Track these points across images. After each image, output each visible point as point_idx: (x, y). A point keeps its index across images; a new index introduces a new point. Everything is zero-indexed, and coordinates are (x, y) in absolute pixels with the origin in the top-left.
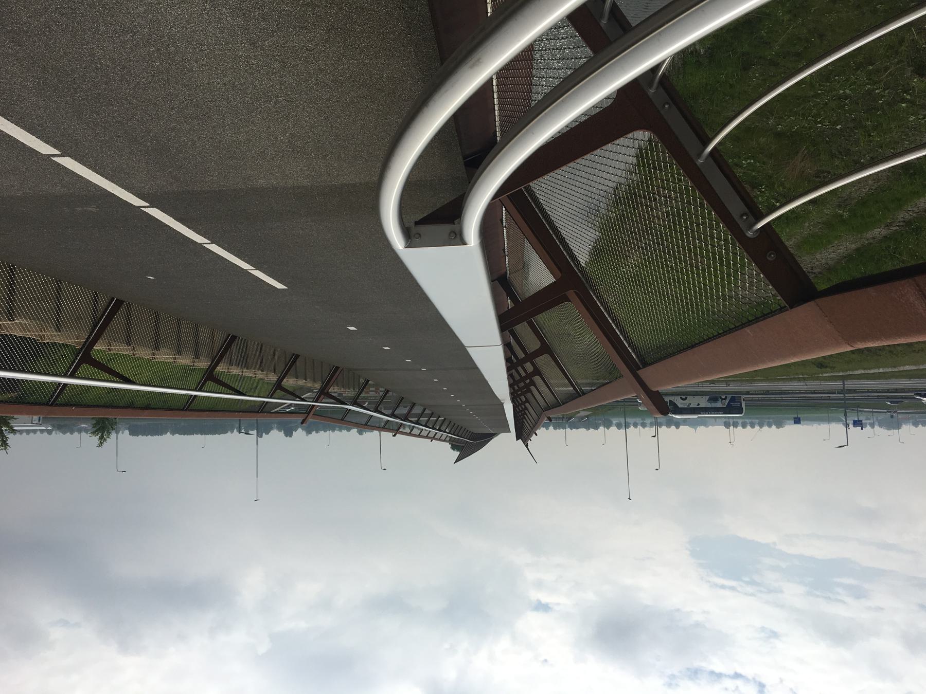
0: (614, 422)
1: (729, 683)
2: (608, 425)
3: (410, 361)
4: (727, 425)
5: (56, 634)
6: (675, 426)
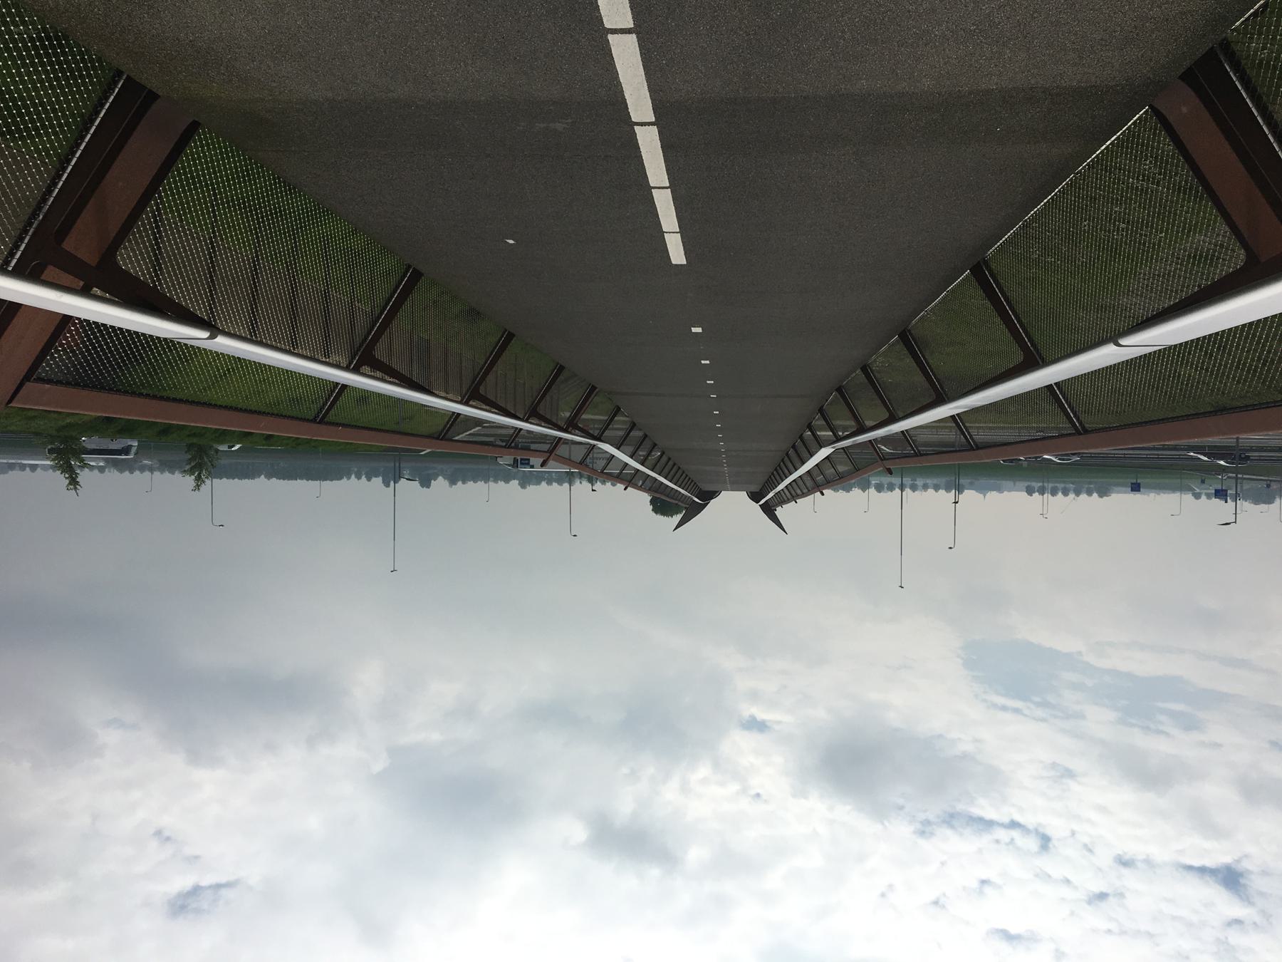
0: (873, 482)
1: (1002, 834)
2: (865, 487)
3: (708, 382)
4: (1030, 491)
5: (111, 737)
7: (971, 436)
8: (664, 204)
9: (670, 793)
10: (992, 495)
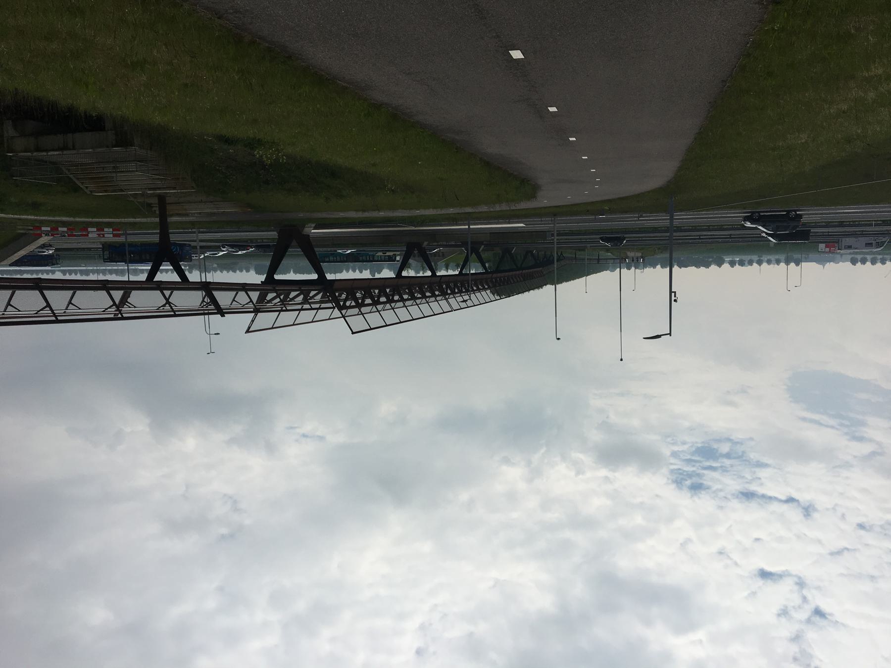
4: (854, 262)
10: (830, 266)
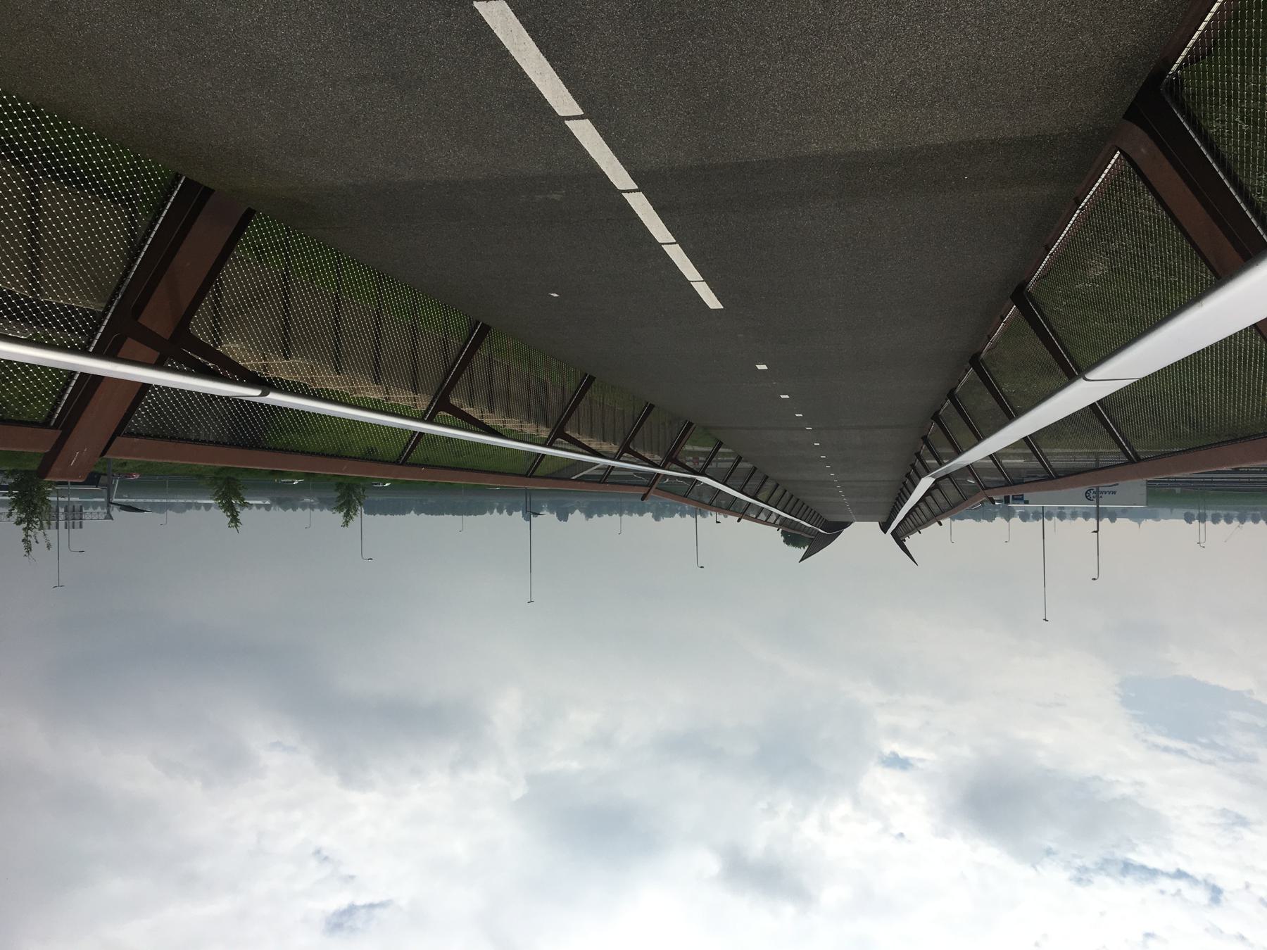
1: (1169, 885)
4: (1189, 519)
5: (274, 760)
6: (319, 508)
7: (1048, 463)
8: (676, 254)
9: (809, 829)
